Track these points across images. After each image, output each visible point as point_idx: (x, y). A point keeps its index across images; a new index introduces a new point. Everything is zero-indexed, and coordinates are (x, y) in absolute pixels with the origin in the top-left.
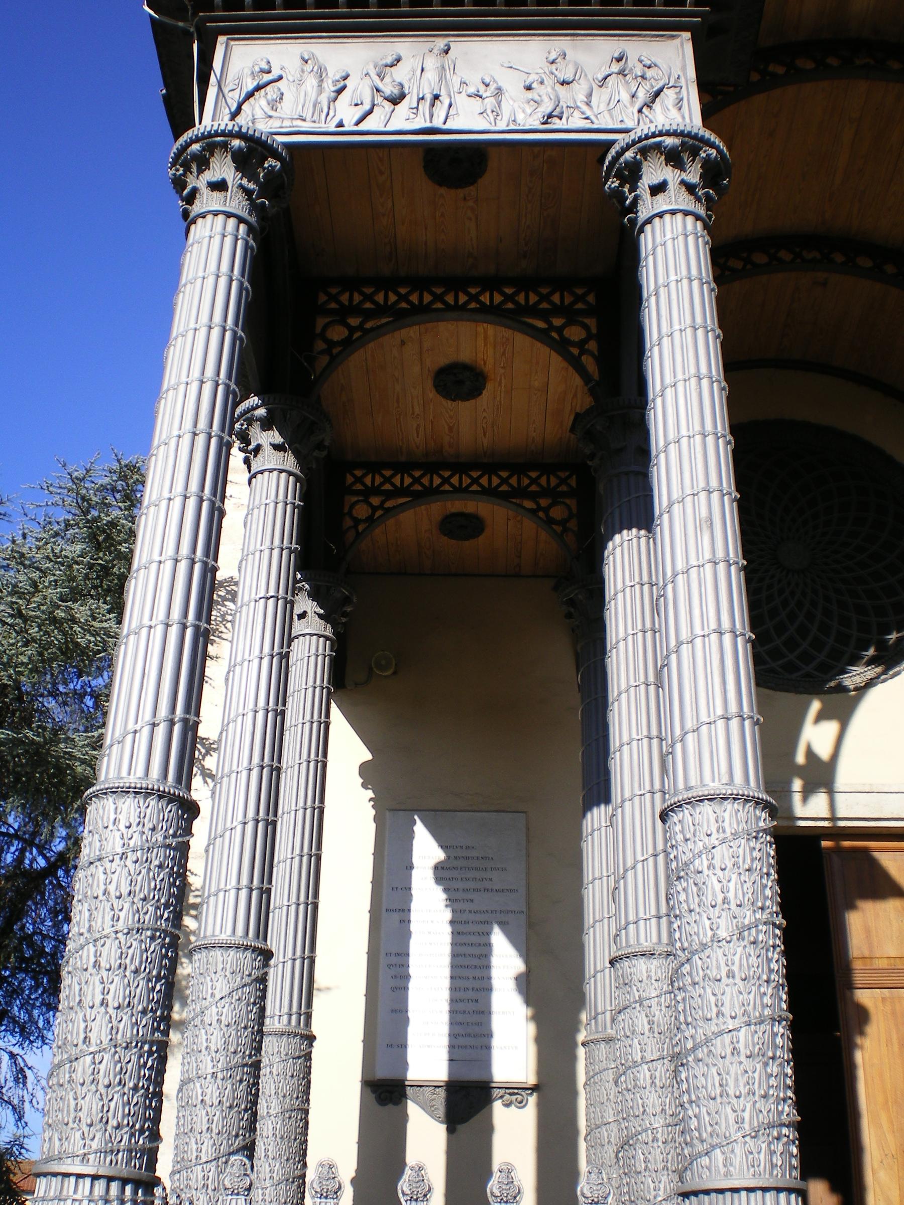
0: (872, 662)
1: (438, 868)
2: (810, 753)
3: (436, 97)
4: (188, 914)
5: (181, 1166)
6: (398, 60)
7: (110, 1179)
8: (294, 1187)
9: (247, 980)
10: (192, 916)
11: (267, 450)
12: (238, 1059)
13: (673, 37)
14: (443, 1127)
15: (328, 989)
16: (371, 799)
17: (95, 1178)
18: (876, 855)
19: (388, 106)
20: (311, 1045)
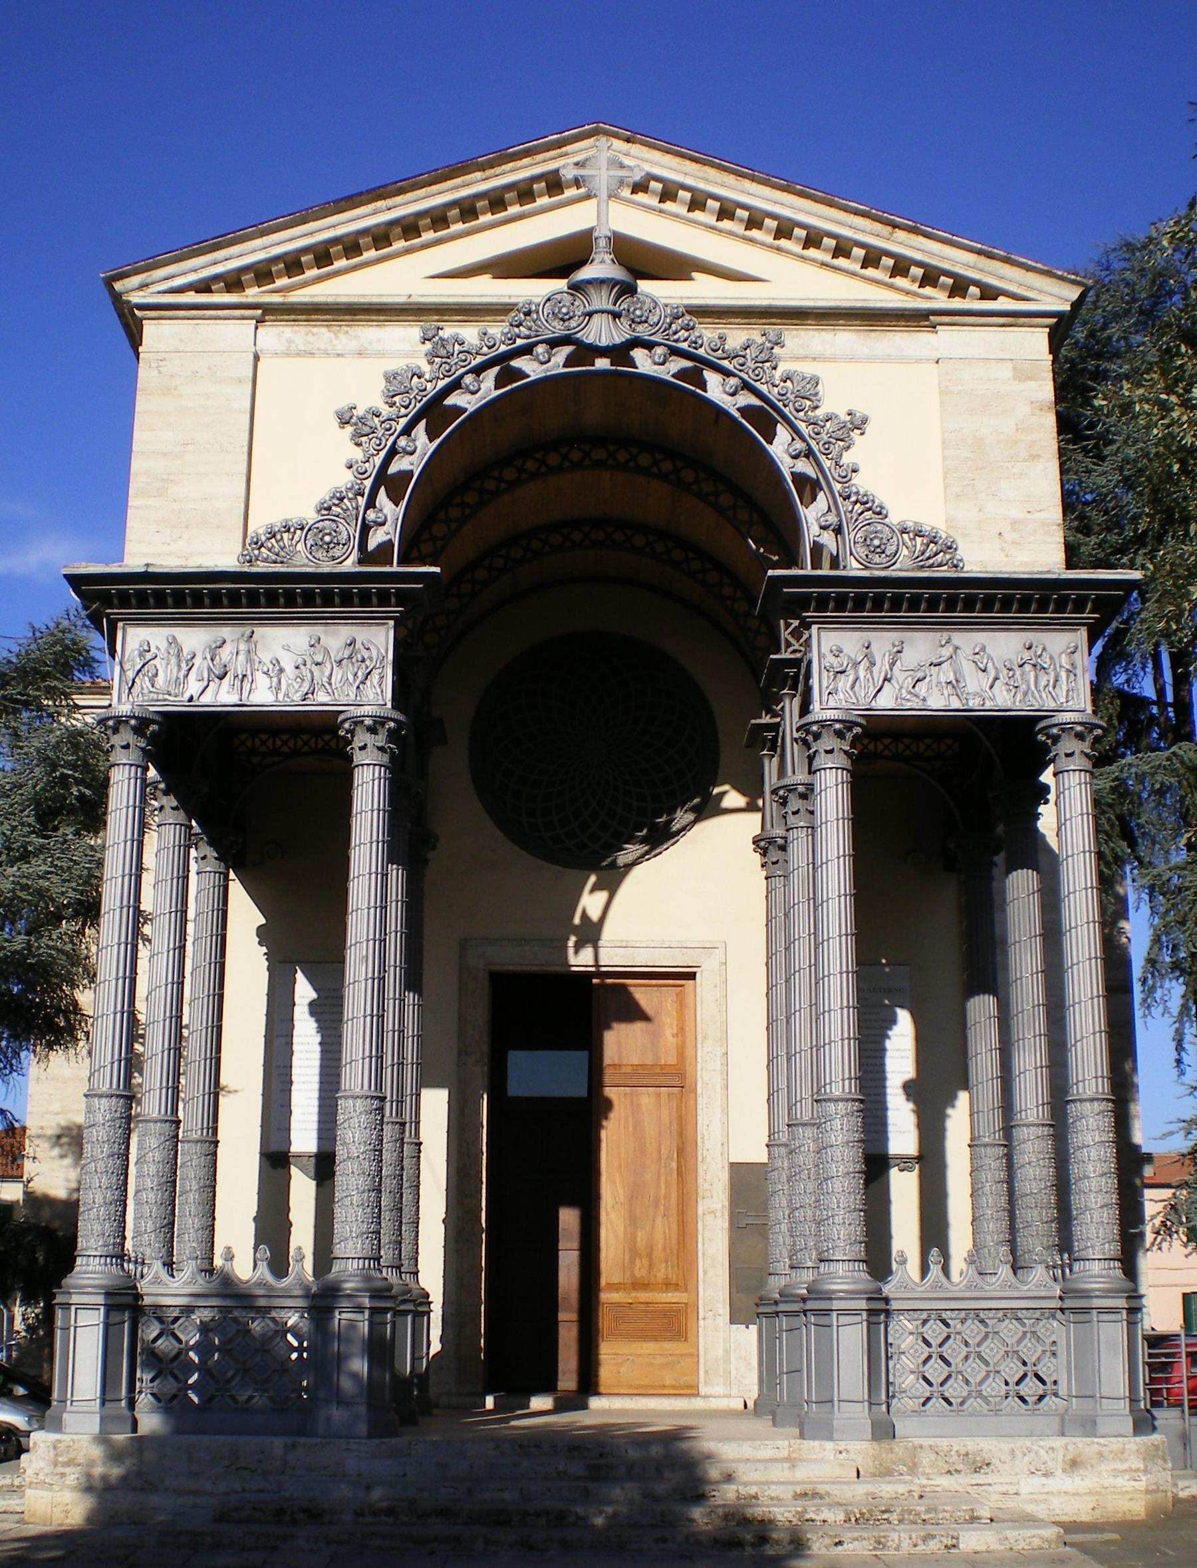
0: (643, 841)
1: (312, 1005)
2: (584, 915)
3: (244, 676)
4: (137, 1042)
5: (137, 1234)
6: (224, 642)
7: (107, 1256)
8: (207, 1232)
9: (167, 1138)
10: (141, 1043)
11: (168, 810)
12: (164, 1179)
13: (384, 624)
14: (314, 1183)
15: (236, 1091)
16: (265, 954)
17: (101, 1256)
18: (632, 989)
19: (217, 680)
20: (217, 1146)
